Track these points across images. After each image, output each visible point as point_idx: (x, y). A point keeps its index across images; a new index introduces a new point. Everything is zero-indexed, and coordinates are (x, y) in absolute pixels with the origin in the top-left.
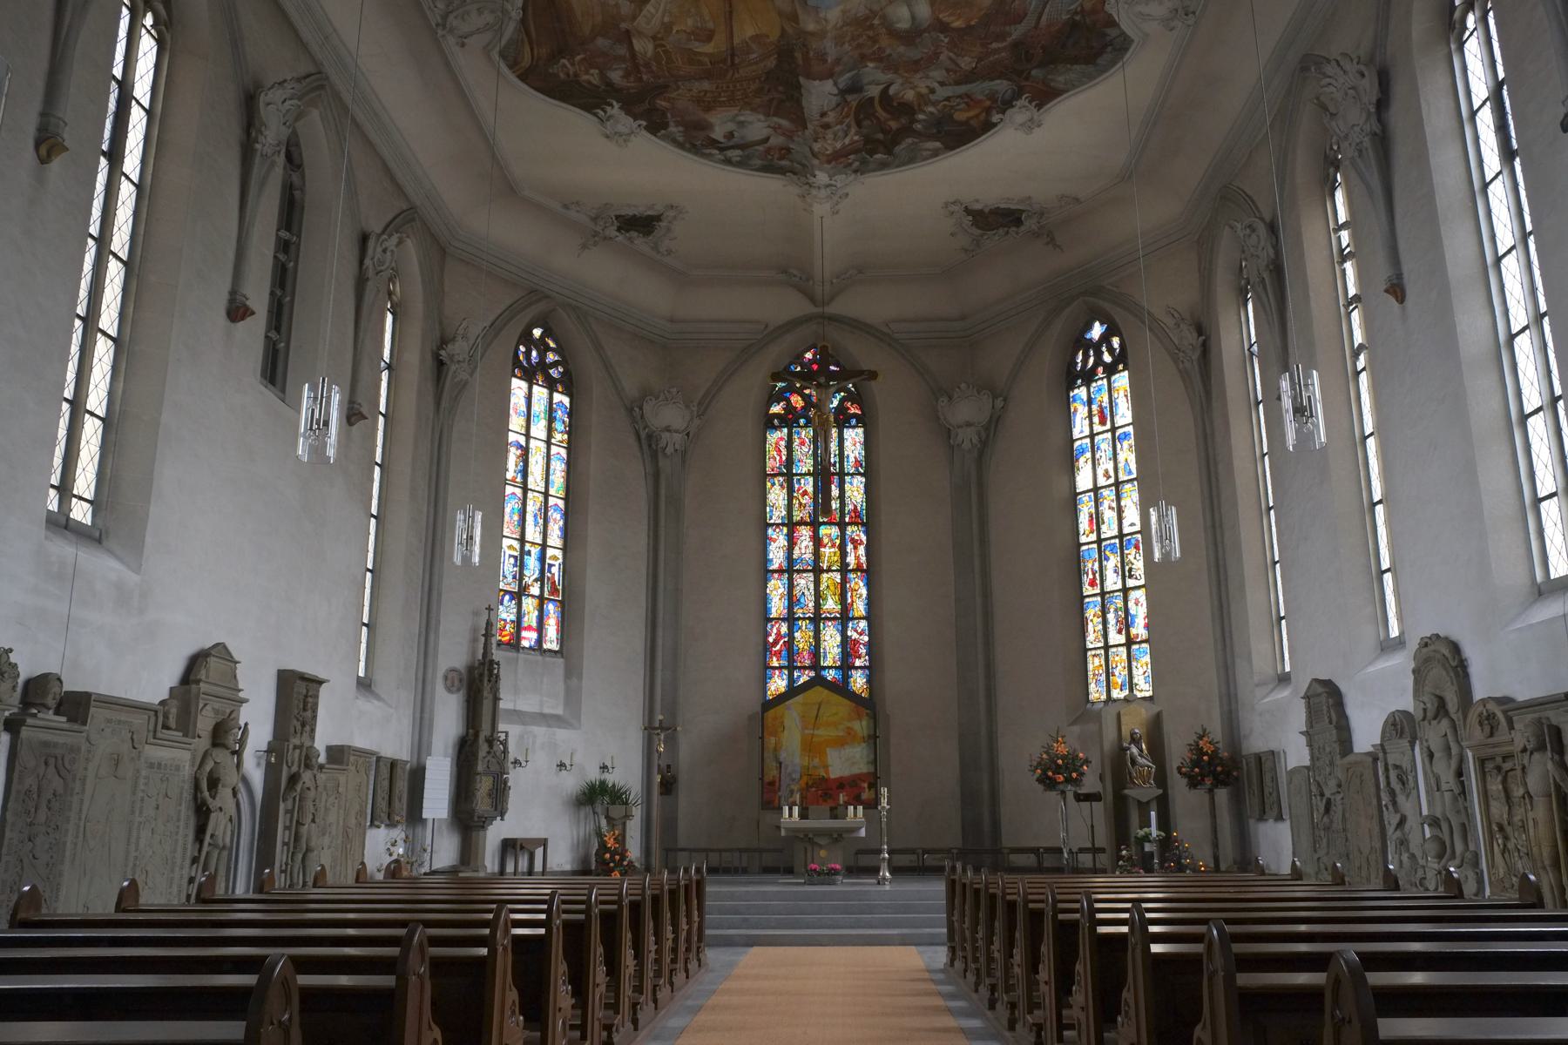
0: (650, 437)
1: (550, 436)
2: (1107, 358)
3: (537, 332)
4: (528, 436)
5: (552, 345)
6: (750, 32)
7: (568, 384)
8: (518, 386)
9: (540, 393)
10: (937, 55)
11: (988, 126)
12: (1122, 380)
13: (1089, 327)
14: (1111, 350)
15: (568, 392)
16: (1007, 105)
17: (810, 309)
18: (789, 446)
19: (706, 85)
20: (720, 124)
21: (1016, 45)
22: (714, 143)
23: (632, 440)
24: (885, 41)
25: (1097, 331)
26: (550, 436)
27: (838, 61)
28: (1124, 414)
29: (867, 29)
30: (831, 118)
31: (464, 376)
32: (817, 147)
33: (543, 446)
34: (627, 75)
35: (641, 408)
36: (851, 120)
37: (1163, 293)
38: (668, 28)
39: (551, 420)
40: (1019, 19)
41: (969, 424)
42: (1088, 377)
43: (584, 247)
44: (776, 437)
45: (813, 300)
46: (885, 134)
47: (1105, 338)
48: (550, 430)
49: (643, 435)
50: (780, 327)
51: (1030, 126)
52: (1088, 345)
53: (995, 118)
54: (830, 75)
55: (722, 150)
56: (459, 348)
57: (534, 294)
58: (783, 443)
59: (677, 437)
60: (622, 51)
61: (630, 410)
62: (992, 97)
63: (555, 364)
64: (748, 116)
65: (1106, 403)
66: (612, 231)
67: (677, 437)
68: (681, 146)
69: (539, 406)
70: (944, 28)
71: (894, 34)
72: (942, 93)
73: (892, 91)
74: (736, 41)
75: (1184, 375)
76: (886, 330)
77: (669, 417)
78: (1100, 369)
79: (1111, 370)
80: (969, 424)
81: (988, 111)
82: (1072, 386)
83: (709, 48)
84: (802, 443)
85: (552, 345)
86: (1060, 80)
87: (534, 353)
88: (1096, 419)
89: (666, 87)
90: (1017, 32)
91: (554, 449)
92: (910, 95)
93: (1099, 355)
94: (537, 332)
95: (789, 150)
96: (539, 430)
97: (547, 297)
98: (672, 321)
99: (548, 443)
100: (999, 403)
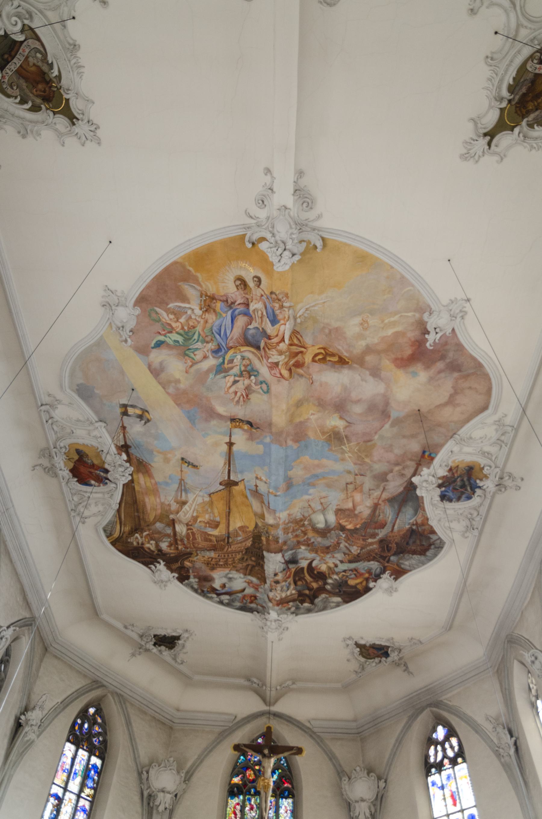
0: (150, 796)
1: (81, 790)
2: (450, 754)
3: (92, 711)
4: (65, 789)
5: (99, 720)
6: (239, 524)
7: (101, 750)
8: (69, 748)
9: (83, 754)
10: (339, 544)
11: (367, 590)
12: (462, 769)
13: (434, 730)
14: (452, 747)
15: (102, 757)
16: (377, 577)
17: (263, 707)
18: (242, 811)
19: (212, 554)
20: (219, 578)
21: (381, 541)
22: (214, 590)
23: (137, 798)
24: (310, 534)
25: (441, 733)
26: (81, 790)
27: (285, 543)
28: (468, 798)
29: (300, 524)
30: (280, 577)
31: (32, 736)
32: (271, 595)
33: (74, 797)
34: (170, 546)
35: (148, 772)
36: (291, 580)
37: (481, 706)
38: (195, 519)
39: (86, 776)
40: (383, 526)
41: (363, 800)
42: (439, 767)
43: (133, 655)
44: (233, 802)
45: (264, 700)
46: (311, 591)
47: (447, 738)
48: (83, 785)
49: (146, 794)
50: (244, 719)
51: (390, 591)
52: (436, 743)
53: (371, 584)
54: (280, 551)
55: (218, 595)
56: (35, 716)
57: (97, 684)
58: (238, 807)
59: (169, 796)
60: (169, 531)
61: (140, 774)
62: (369, 572)
63: (99, 734)
64: (234, 574)
65: (454, 789)
66: (150, 646)
67: (169, 796)
68: (196, 591)
69: (79, 767)
70: (342, 528)
71: (316, 530)
72: (342, 567)
73: (314, 564)
74: (231, 529)
75: (506, 767)
76: (308, 725)
77: (165, 780)
78: (446, 761)
79: (454, 762)
80: (363, 800)
81: (367, 580)
82: (428, 773)
83: (216, 532)
84: (252, 808)
85: (99, 720)
86: (406, 564)
87: (86, 726)
88: (449, 801)
89: (190, 554)
90: (382, 533)
91: (82, 802)
92: (324, 568)
93: (444, 750)
94: (92, 711)
95: (255, 597)
96: (74, 785)
97: (103, 686)
98: (178, 710)
99: (79, 796)
100: (382, 784)
